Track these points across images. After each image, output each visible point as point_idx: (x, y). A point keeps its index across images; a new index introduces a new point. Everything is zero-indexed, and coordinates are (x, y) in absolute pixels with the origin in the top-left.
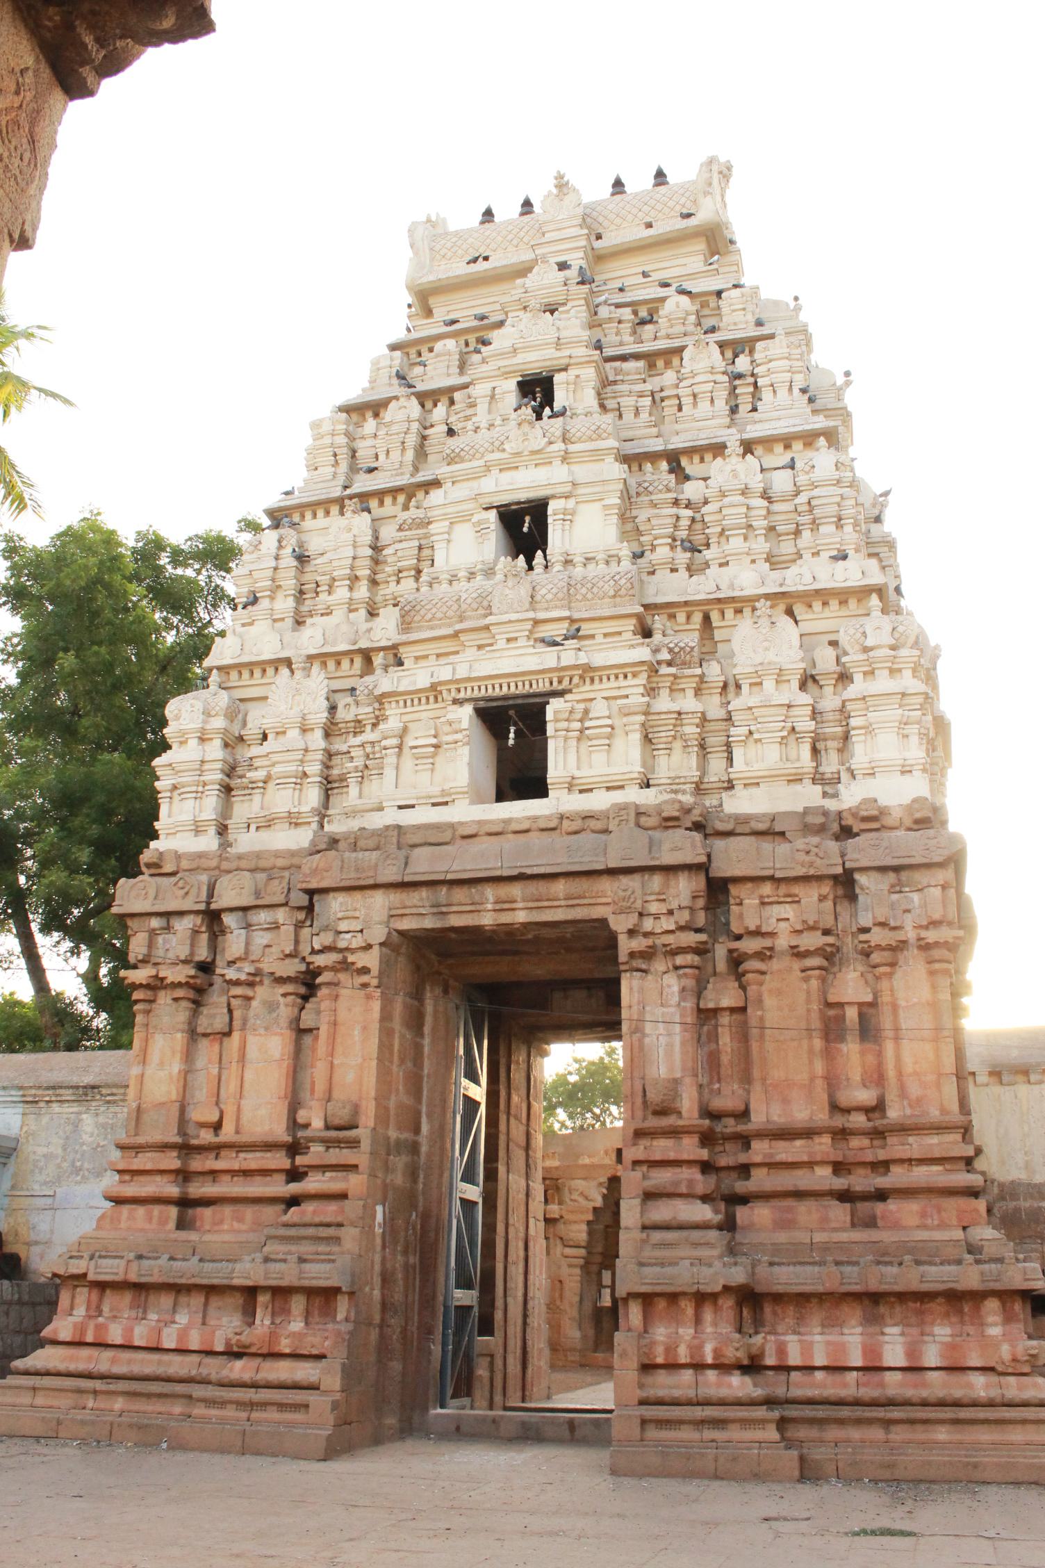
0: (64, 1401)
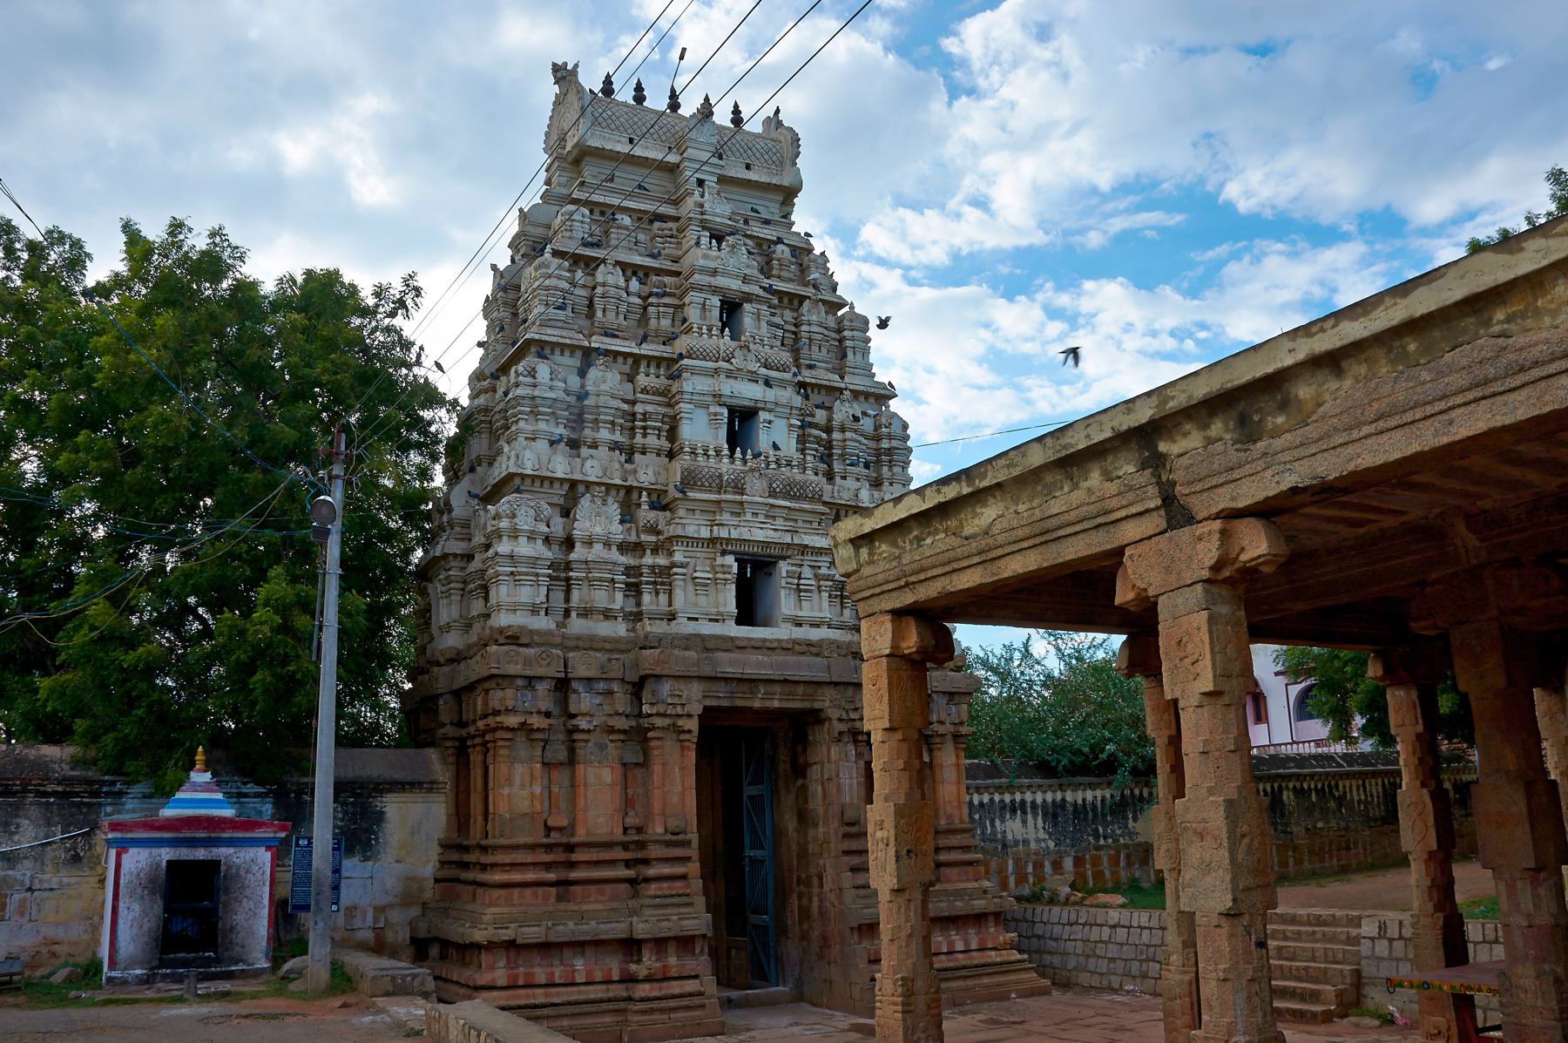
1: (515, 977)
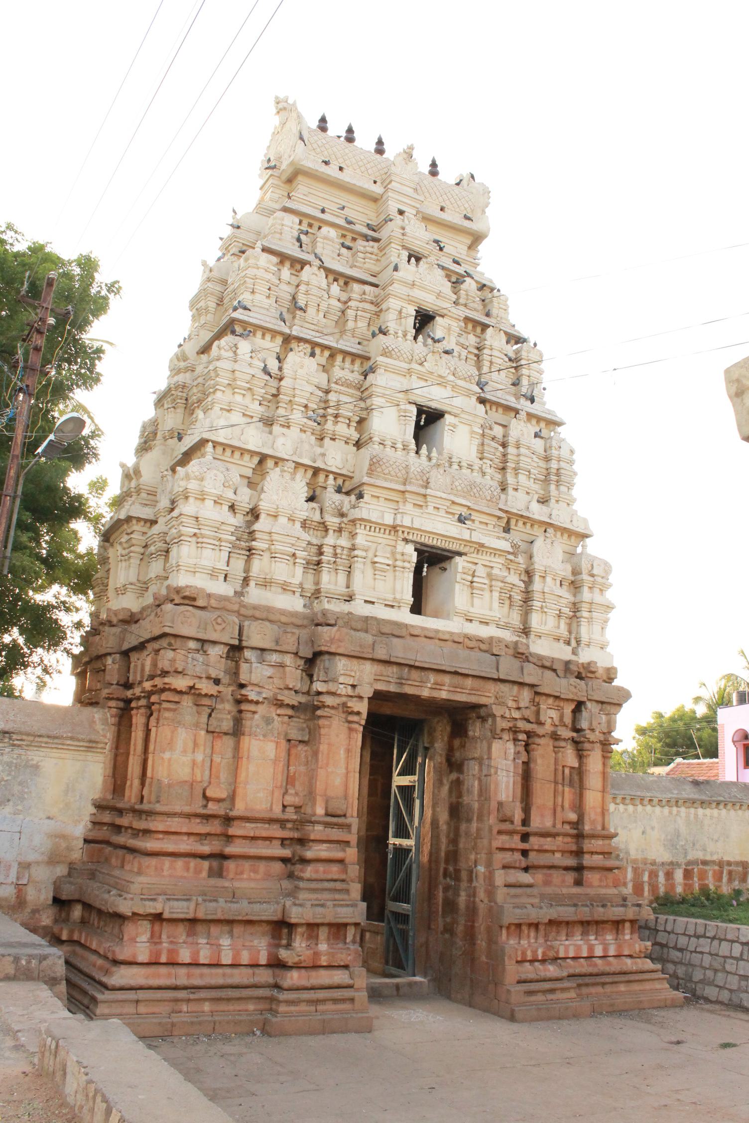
0: (164, 1009)
1: (158, 954)
